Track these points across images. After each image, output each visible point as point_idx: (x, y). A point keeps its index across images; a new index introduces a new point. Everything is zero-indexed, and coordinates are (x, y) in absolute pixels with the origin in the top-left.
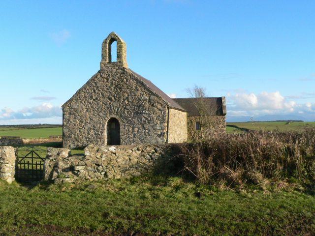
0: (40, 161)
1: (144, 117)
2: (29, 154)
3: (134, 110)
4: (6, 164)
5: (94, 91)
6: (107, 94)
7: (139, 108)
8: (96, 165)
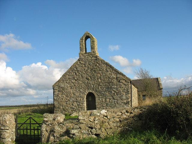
0: (38, 127)
1: (113, 90)
2: (28, 120)
3: (106, 86)
4: (6, 131)
5: (76, 73)
6: (85, 76)
7: (109, 84)
8: (89, 127)
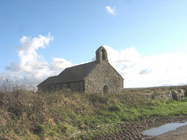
5: (98, 72)
